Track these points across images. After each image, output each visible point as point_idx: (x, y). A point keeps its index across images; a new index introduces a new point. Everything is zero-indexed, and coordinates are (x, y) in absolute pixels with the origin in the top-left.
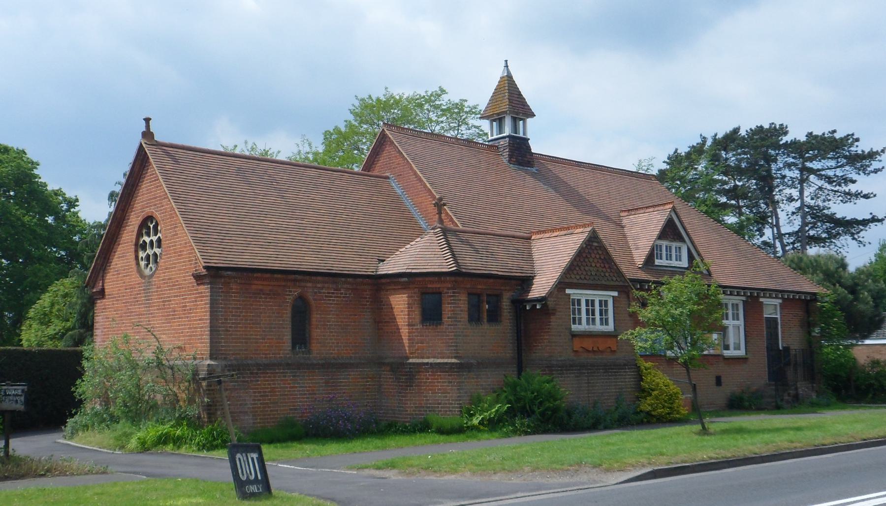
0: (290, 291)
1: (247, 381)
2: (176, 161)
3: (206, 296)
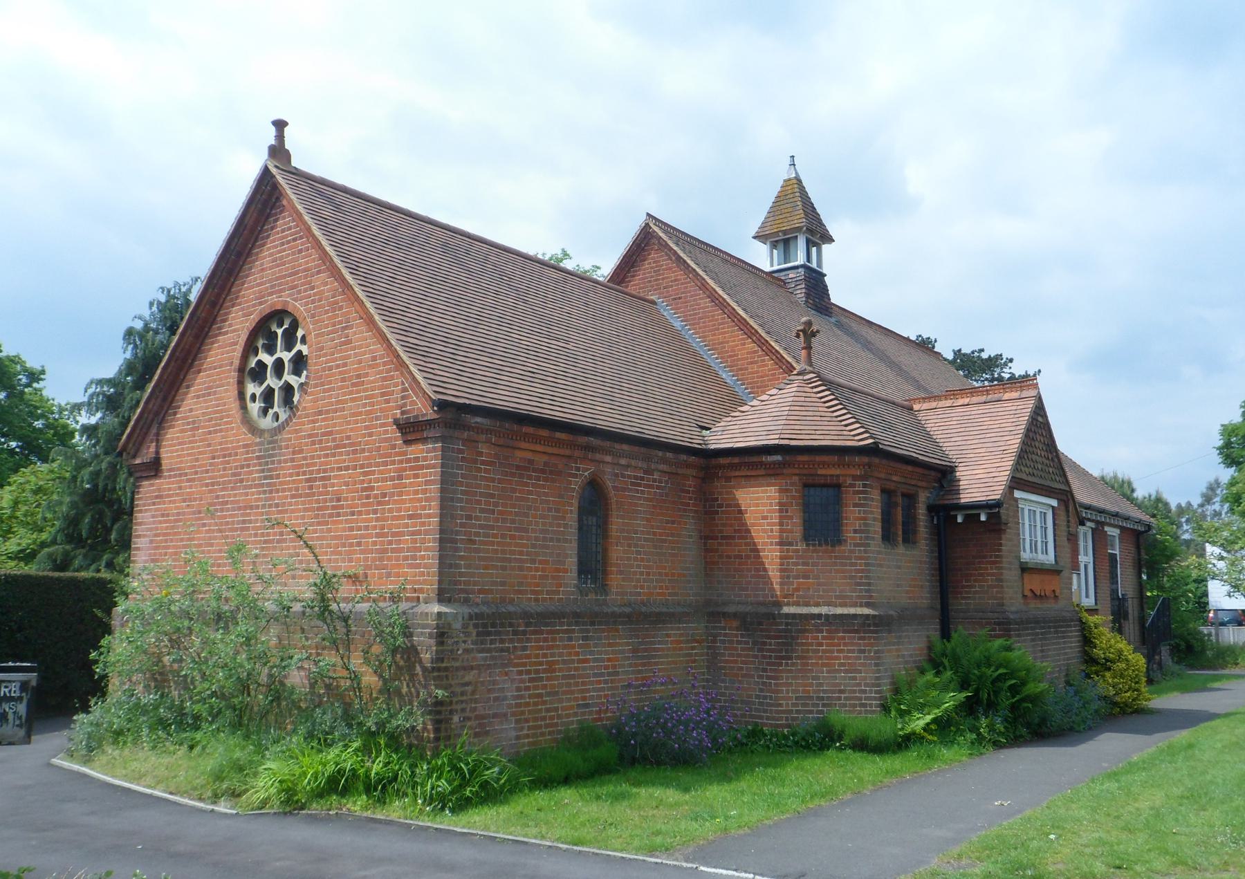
0: (578, 469)
1: (508, 650)
2: (338, 208)
3: (434, 466)
